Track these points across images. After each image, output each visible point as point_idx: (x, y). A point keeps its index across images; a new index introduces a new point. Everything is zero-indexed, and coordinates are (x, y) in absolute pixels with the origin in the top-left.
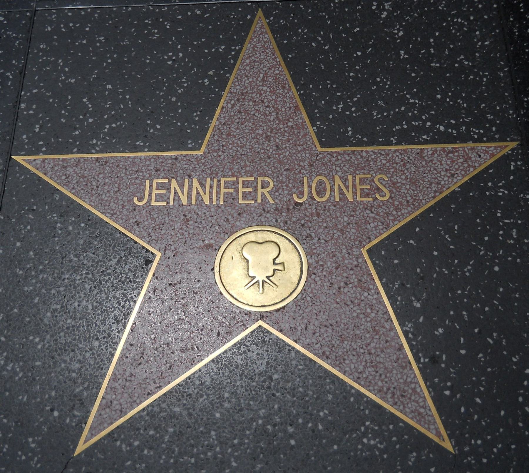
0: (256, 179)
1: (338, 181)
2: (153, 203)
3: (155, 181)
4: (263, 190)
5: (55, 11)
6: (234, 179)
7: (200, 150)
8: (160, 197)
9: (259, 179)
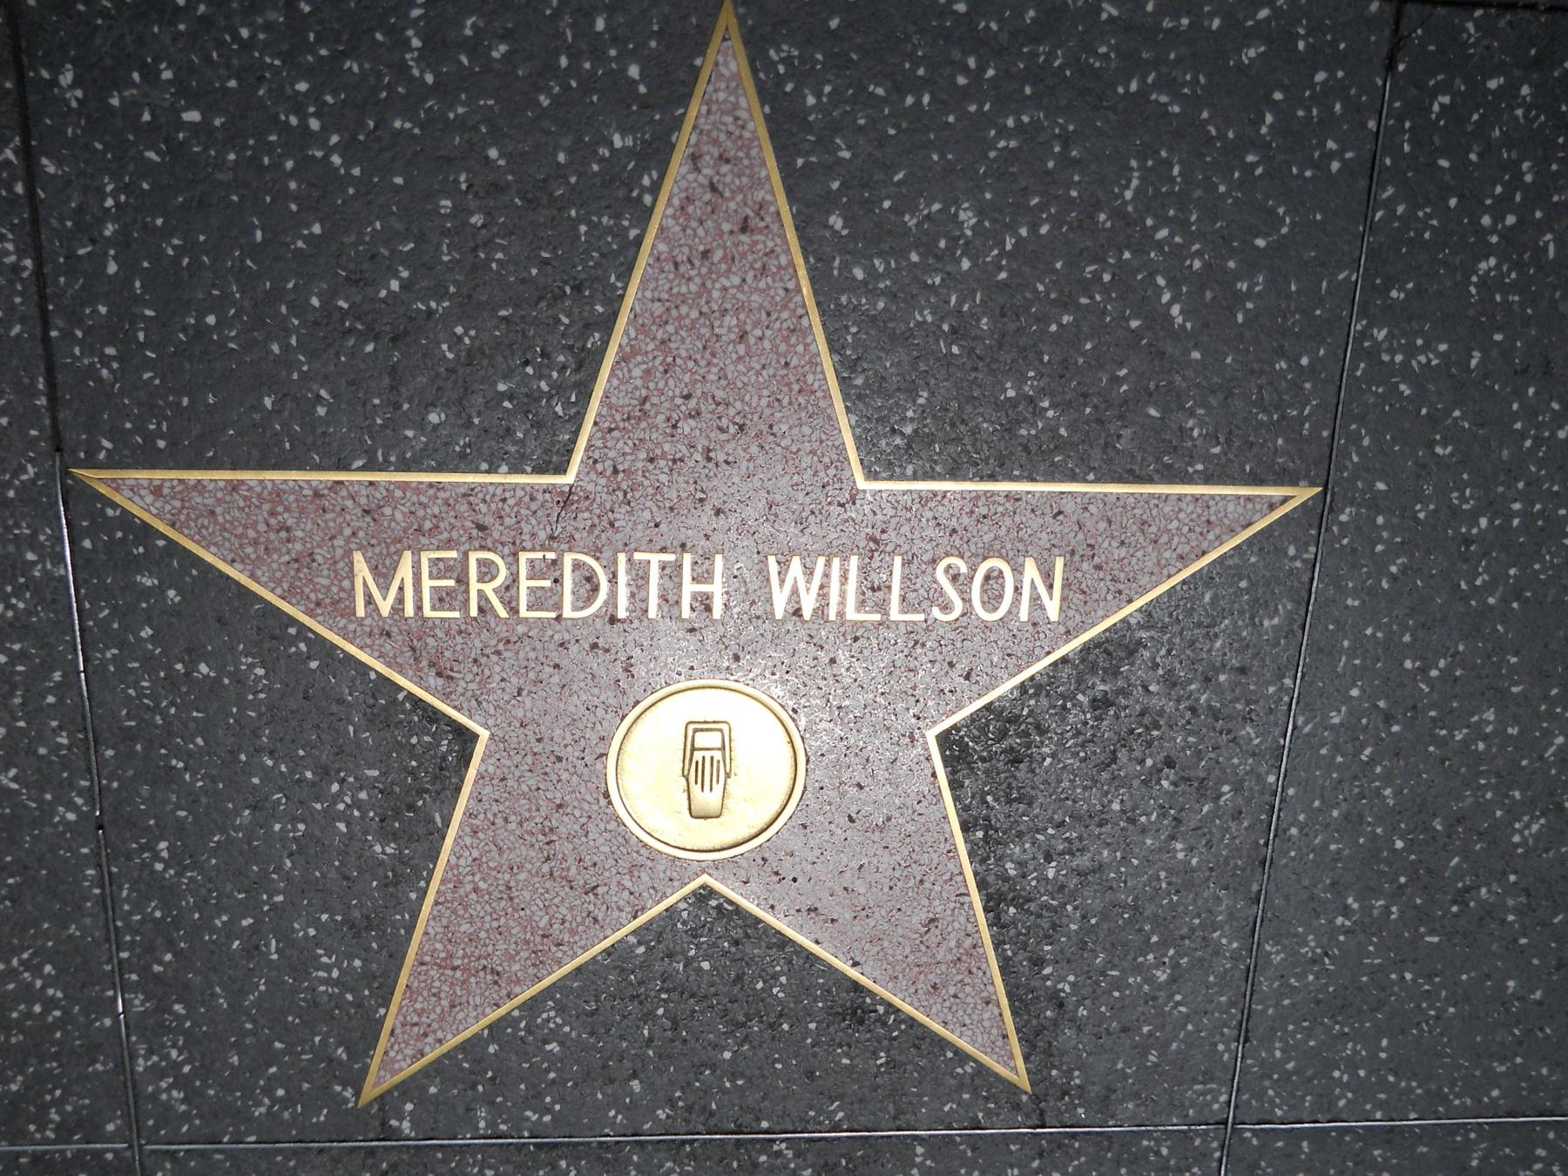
0: (466, 554)
1: (1031, 571)
2: (428, 612)
3: (524, 557)
4: (481, 586)
5: (1354, 278)
6: (551, 556)
7: (565, 472)
8: (441, 599)
9: (473, 557)
